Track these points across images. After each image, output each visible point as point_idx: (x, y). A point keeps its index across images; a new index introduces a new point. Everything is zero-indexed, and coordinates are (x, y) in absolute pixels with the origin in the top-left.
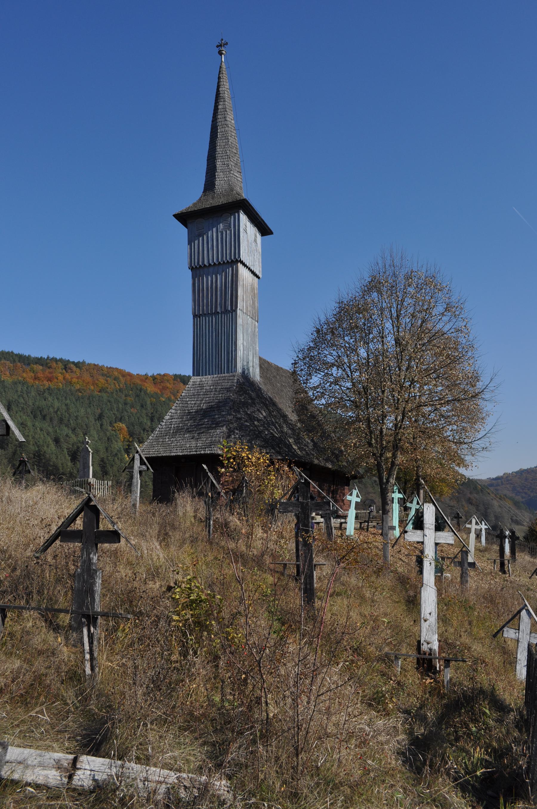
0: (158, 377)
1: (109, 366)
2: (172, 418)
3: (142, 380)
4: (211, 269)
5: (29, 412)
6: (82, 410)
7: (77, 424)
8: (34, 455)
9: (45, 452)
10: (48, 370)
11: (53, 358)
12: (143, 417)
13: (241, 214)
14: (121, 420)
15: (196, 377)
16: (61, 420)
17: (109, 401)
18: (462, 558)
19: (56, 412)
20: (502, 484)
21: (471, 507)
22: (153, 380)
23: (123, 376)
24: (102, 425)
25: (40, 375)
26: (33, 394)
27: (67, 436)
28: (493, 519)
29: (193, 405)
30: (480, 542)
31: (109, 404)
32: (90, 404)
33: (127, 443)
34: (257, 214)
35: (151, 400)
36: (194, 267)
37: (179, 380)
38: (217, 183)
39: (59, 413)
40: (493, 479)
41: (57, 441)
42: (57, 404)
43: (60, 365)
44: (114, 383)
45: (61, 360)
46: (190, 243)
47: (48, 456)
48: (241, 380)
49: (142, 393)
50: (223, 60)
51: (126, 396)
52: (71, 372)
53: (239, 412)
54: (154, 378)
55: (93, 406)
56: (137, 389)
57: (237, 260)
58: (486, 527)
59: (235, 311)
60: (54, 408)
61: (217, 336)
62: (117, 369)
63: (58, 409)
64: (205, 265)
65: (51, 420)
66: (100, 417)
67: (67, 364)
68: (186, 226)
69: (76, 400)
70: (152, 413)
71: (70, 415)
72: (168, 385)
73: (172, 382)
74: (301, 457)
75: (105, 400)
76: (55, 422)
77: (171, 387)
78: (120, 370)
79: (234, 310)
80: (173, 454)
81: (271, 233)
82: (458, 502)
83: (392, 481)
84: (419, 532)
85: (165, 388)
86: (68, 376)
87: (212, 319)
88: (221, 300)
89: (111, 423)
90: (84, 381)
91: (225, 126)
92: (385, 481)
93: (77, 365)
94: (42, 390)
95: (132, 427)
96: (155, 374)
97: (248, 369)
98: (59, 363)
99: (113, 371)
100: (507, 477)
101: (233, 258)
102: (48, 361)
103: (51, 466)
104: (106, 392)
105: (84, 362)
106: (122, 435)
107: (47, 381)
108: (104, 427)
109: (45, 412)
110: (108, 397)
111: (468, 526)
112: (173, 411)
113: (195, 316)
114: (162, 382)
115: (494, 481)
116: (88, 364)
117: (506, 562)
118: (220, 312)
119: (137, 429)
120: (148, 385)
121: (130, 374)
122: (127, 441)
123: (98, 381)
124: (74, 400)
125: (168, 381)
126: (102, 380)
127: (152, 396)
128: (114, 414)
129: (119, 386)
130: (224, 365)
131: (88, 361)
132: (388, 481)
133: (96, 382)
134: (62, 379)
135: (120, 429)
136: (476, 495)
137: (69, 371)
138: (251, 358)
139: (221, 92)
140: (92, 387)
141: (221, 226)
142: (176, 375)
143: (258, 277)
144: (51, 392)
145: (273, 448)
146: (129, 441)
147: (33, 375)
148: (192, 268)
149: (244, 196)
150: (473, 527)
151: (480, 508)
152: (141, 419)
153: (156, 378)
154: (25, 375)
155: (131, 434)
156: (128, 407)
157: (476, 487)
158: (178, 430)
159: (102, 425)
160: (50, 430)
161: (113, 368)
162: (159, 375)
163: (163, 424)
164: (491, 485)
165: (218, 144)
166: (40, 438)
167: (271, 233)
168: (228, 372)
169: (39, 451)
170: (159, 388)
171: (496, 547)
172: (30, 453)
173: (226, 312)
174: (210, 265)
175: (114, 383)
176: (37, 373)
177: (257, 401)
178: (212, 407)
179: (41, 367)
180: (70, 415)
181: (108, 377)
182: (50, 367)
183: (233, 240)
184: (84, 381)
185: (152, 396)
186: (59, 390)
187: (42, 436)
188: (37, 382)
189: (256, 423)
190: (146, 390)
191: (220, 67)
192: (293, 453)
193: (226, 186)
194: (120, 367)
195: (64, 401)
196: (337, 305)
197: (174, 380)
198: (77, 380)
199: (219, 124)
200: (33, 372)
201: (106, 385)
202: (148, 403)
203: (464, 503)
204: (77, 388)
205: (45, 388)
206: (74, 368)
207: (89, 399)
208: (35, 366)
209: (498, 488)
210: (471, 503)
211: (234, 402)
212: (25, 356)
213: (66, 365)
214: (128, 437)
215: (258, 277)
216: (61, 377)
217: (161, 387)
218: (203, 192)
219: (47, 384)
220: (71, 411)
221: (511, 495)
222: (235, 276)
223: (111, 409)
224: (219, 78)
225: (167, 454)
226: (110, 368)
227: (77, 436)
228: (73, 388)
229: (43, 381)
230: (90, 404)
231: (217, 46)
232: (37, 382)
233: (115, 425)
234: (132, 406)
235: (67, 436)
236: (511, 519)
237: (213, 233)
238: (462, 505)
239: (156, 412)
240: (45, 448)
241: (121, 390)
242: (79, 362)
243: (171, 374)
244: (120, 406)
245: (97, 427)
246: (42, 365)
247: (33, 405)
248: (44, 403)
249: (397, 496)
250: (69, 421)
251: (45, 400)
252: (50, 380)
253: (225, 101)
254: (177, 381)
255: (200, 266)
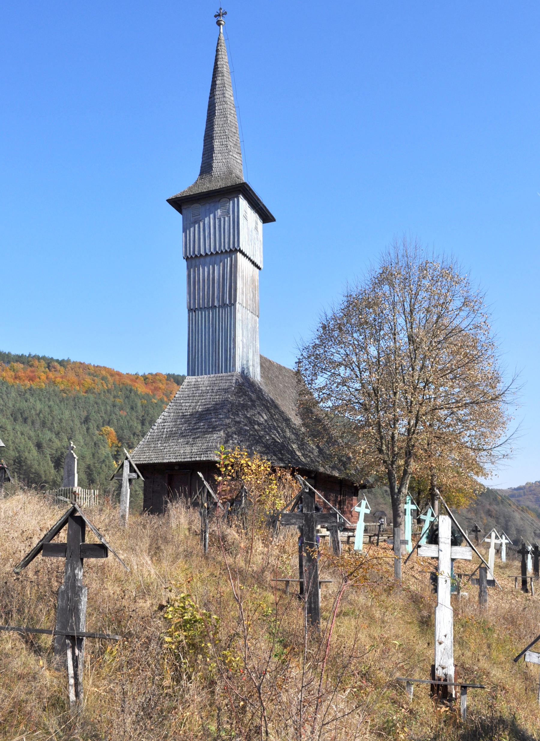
0: (150, 376)
1: (96, 365)
2: (165, 421)
3: (132, 380)
4: (208, 259)
5: (9, 414)
6: (67, 413)
7: (61, 428)
8: (15, 461)
9: (26, 458)
10: (30, 369)
11: (34, 356)
12: (133, 421)
13: (240, 199)
14: (109, 423)
15: (191, 377)
16: (44, 424)
17: (96, 403)
18: (481, 575)
19: (38, 415)
20: (525, 494)
21: (490, 520)
22: (145, 380)
23: (112, 375)
24: (88, 429)
25: (21, 374)
26: (13, 394)
27: (50, 440)
28: (515, 533)
29: (188, 408)
30: (500, 557)
31: (96, 405)
32: (75, 405)
33: (116, 449)
34: (251, 189)
35: (142, 402)
36: (190, 257)
37: (172, 380)
38: (214, 165)
39: (41, 415)
40: (515, 489)
41: (39, 446)
42: (39, 406)
43: (43, 363)
44: (102, 383)
45: (44, 358)
46: (184, 231)
47: (29, 462)
48: (241, 380)
49: (133, 394)
50: (222, 31)
51: (114, 397)
52: (55, 371)
53: (238, 415)
54: (145, 378)
55: (79, 408)
56: (127, 389)
57: (236, 249)
58: (507, 541)
59: (234, 305)
60: (36, 410)
61: (214, 331)
62: (105, 368)
63: (40, 412)
64: (201, 255)
65: (33, 423)
66: (86, 420)
67: (51, 362)
68: (181, 212)
69: (61, 402)
70: (143, 416)
71: (53, 418)
72: (161, 385)
73: (165, 382)
74: (305, 465)
75: (91, 402)
76: (37, 425)
77: (164, 388)
78: (108, 368)
79: (232, 304)
80: (165, 461)
81: (273, 220)
82: (476, 514)
83: (405, 491)
84: (433, 547)
85: (157, 389)
86: (51, 375)
87: (209, 313)
88: (219, 293)
89: (98, 427)
90: (68, 381)
91: (224, 103)
92: (396, 490)
93: (61, 363)
94: (23, 391)
95: (121, 432)
96: (146, 374)
97: (248, 369)
98: (42, 361)
99: (100, 370)
100: (530, 487)
101: (231, 247)
102: (30, 359)
103: (33, 473)
104: (93, 393)
105: (68, 361)
106: (110, 440)
107: (29, 380)
108: (90, 431)
109: (26, 415)
110: (95, 398)
111: (487, 540)
112: (166, 414)
113: (190, 310)
114: (154, 382)
115: (515, 492)
116: (74, 362)
117: (529, 580)
118: (217, 306)
119: (127, 433)
120: (139, 386)
121: (119, 374)
122: (116, 447)
123: (84, 380)
124: (58, 402)
125: (160, 381)
126: (88, 380)
127: (143, 398)
128: (102, 417)
129: (107, 386)
130: (222, 364)
131: (73, 359)
132: (400, 491)
133: (82, 381)
134: (45, 379)
135: (108, 434)
136: (495, 507)
137: (53, 370)
138: (251, 356)
139: (219, 66)
140: (78, 388)
141: (219, 212)
142: (169, 374)
143: (259, 268)
144: (33, 392)
145: (275, 455)
146: (117, 446)
147: (13, 374)
148: (187, 258)
149: (244, 180)
150: (493, 541)
151: (500, 521)
152: (131, 423)
153: (147, 378)
154: (4, 374)
155: (120, 439)
156: (117, 410)
157: (496, 498)
158: (171, 435)
159: (88, 429)
160: (32, 434)
161: (100, 367)
162: (151, 374)
163: (155, 428)
164: (513, 496)
165: (216, 123)
166: (20, 443)
167: (273, 220)
168: (226, 372)
169: (20, 456)
170: (150, 389)
171: (518, 564)
172: (10, 459)
173: (224, 305)
174: (206, 254)
175: (102, 383)
176: (17, 371)
177: (258, 403)
178: (208, 410)
179: (22, 366)
180: (53, 418)
181: (95, 376)
182: (31, 366)
183: (231, 227)
184: (68, 381)
185: (143, 398)
186: (41, 390)
187: (23, 440)
188: (18, 382)
189: (256, 427)
190: (137, 390)
191: (219, 39)
192: (297, 460)
193: (224, 169)
194: (108, 366)
195: (47, 402)
196: (345, 299)
197: (167, 380)
198: (61, 380)
199: (217, 100)
200: (14, 371)
201: (93, 385)
202: (139, 404)
203: (483, 515)
204: (61, 389)
205: (27, 388)
206: (58, 367)
207: (74, 400)
208: (15, 364)
209: (520, 498)
210: (491, 516)
211: (232, 404)
212: (5, 353)
213: (49, 363)
214: (117, 442)
215: (259, 268)
216: (43, 376)
217: (153, 388)
218: (200, 175)
219: (28, 383)
220: (54, 413)
221: (534, 507)
222: (234, 267)
223: (98, 412)
224: (217, 51)
225: (160, 461)
226: (97, 366)
227: (61, 440)
228: (56, 388)
229: (24, 381)
230: (75, 405)
231: (216, 16)
232: (18, 382)
233: (103, 429)
234: (121, 409)
235: (50, 440)
236: (534, 533)
237: (210, 220)
238: (481, 518)
239: (148, 415)
240: (27, 454)
241: (109, 391)
242: (63, 360)
243: (164, 373)
244: (108, 408)
245: (83, 431)
246: (23, 363)
247: (14, 406)
248: (25, 404)
249: (409, 507)
250: (52, 424)
251: (26, 401)
252: (32, 379)
253: (223, 76)
254: (170, 381)
255: (196, 256)
